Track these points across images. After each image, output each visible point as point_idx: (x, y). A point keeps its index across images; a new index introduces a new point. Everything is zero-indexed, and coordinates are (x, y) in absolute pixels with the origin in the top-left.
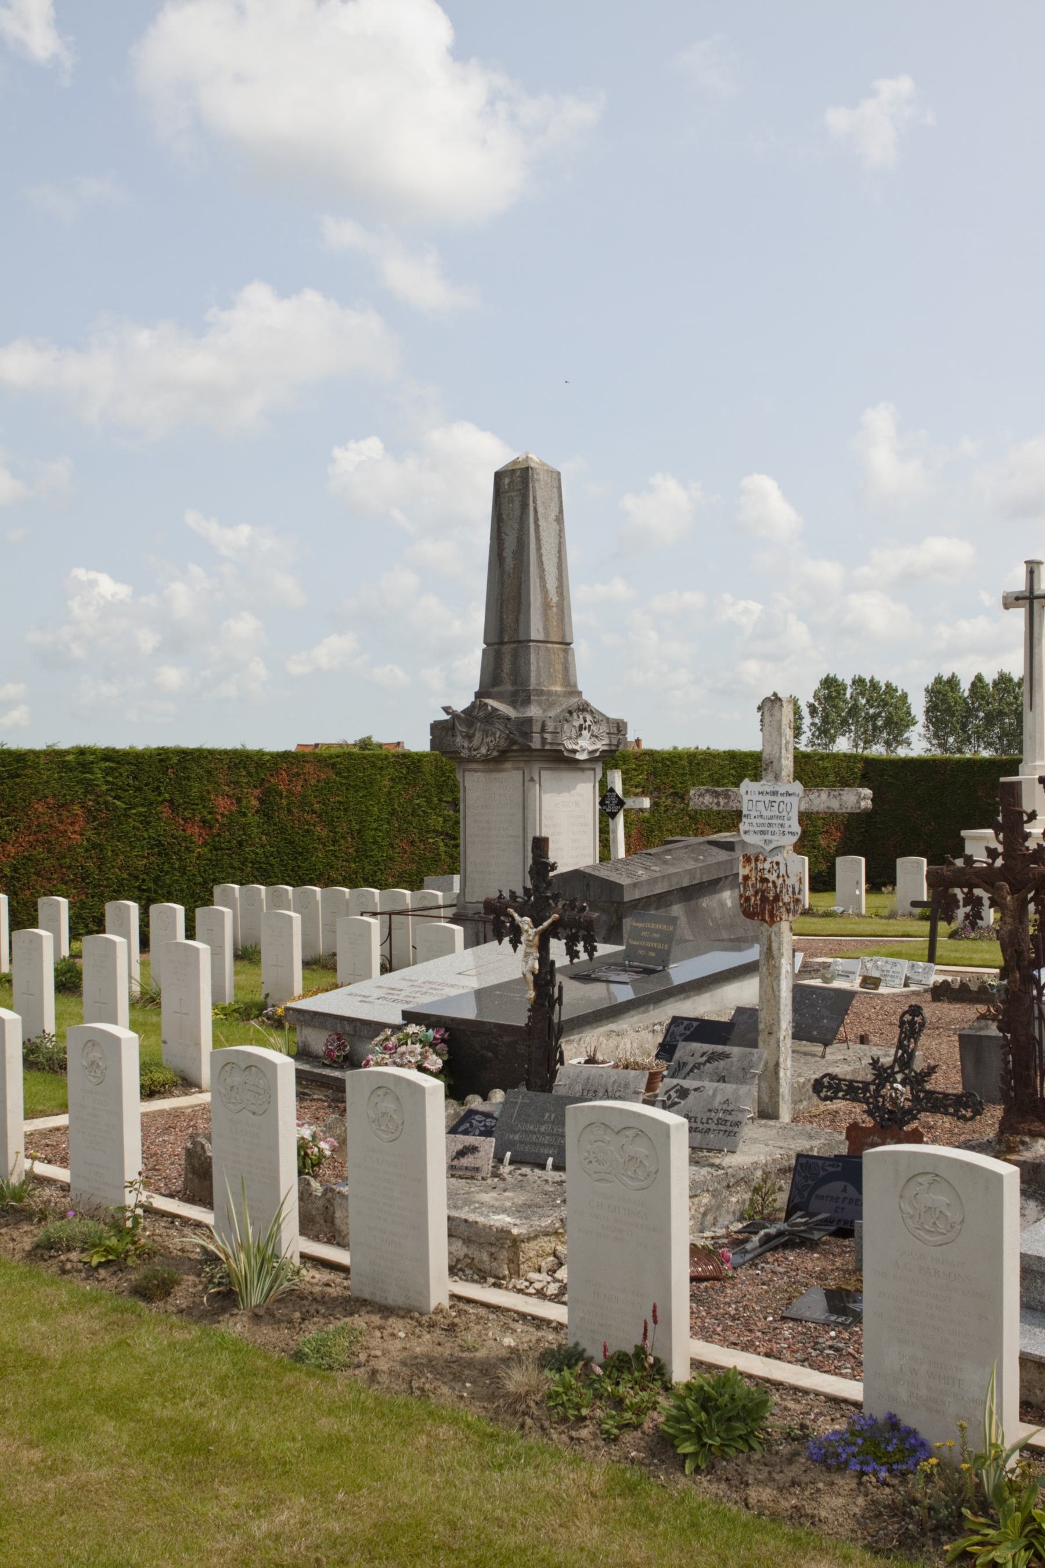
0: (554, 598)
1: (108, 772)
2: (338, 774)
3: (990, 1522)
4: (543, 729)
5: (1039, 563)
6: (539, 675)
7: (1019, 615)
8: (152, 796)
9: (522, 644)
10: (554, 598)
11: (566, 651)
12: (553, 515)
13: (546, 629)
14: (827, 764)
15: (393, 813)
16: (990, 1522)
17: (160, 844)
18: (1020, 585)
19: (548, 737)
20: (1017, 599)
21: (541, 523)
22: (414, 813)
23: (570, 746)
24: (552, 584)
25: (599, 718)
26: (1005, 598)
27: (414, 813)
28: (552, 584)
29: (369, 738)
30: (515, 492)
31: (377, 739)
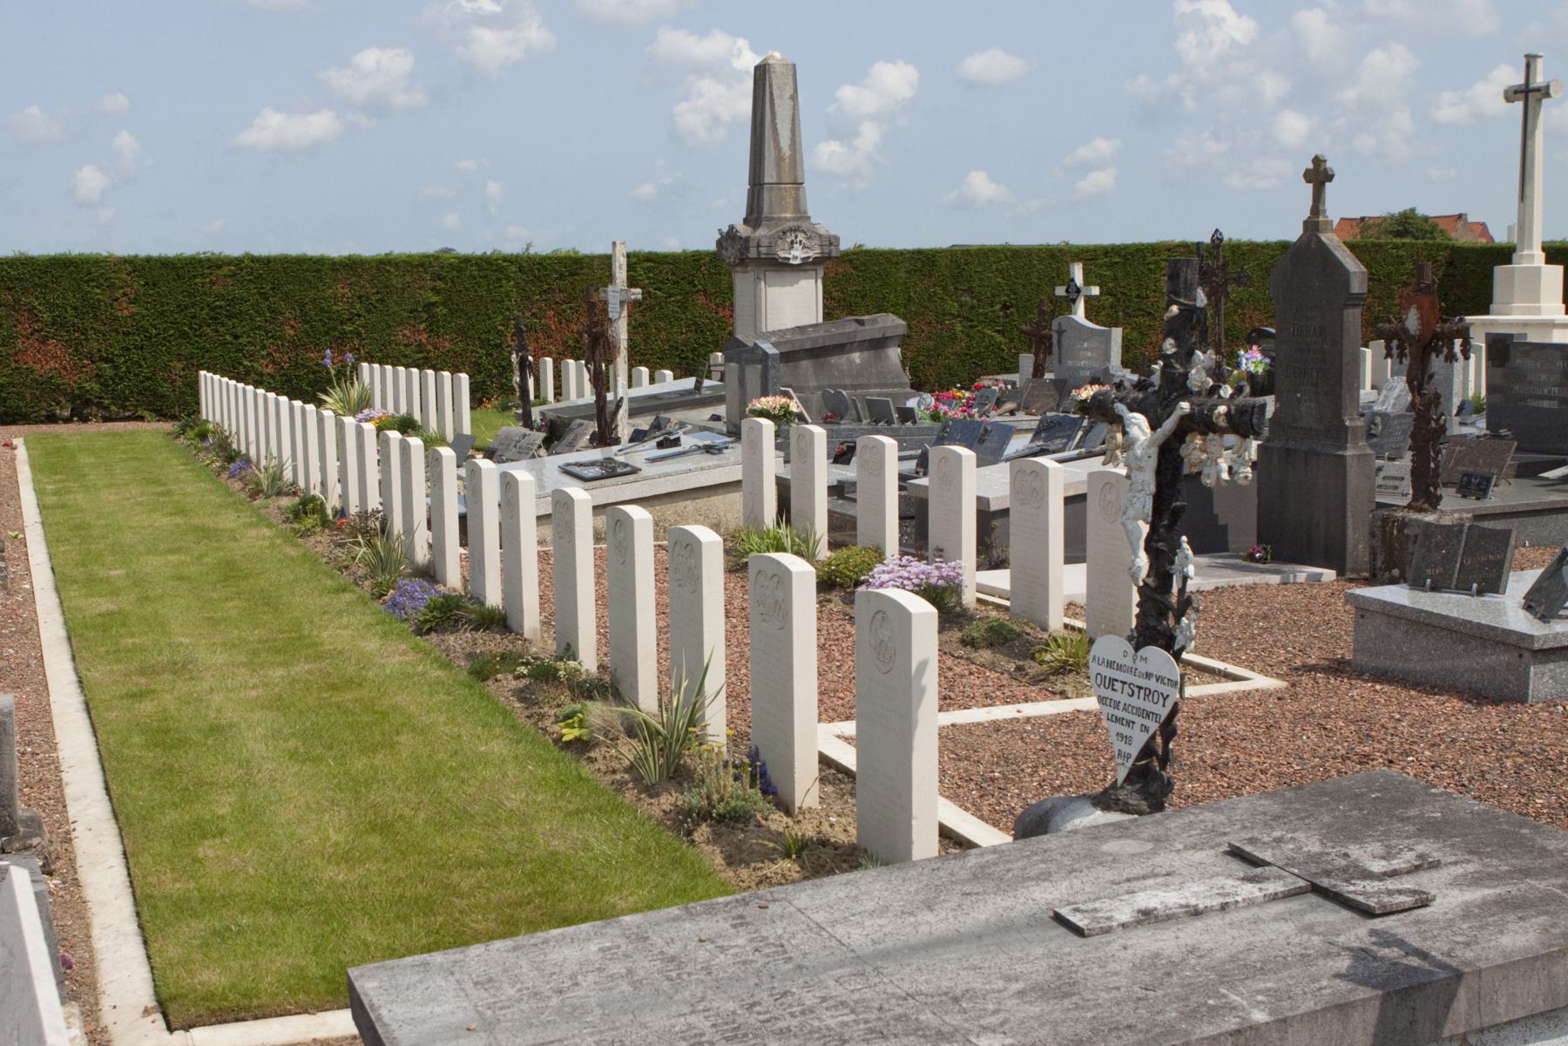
0: (786, 151)
1: (649, 270)
2: (855, 268)
3: (1526, 862)
4: (759, 246)
5: (1536, 57)
6: (771, 206)
7: (1519, 105)
8: (688, 288)
9: (762, 185)
10: (786, 151)
11: (797, 190)
12: (789, 91)
13: (779, 174)
14: (1401, 252)
15: (910, 299)
16: (1526, 862)
17: (695, 323)
18: (1519, 80)
19: (763, 250)
20: (1516, 92)
21: (777, 101)
22: (930, 299)
23: (782, 254)
24: (785, 142)
25: (811, 234)
26: (1506, 92)
27: (930, 299)
28: (785, 142)
29: (1413, 210)
30: (762, 73)
31: (1420, 212)
